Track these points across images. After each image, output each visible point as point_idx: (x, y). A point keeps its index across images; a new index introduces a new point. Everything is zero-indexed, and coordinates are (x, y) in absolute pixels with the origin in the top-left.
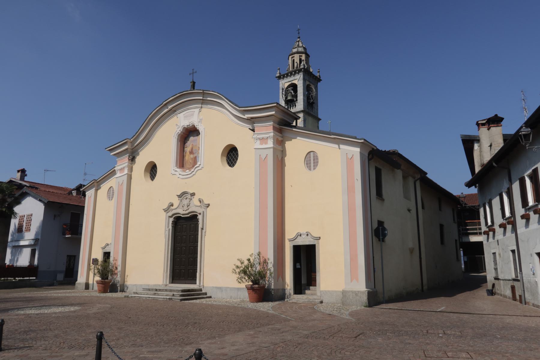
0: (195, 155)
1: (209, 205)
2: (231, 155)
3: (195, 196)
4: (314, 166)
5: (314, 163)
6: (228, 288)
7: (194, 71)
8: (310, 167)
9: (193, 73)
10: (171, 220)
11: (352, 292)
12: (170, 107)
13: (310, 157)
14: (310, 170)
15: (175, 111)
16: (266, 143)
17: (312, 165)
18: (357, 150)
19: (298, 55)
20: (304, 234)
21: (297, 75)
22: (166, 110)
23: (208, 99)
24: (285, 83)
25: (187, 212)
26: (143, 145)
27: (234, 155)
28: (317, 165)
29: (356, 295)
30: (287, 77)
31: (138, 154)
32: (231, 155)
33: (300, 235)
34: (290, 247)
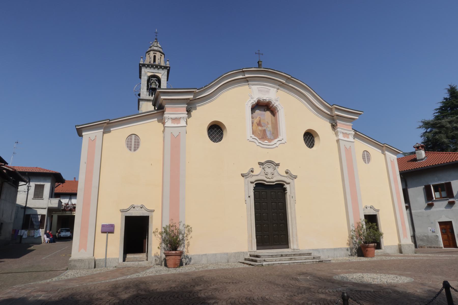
0: (263, 128)
1: (243, 175)
2: (310, 137)
3: (279, 167)
4: (368, 161)
5: (368, 159)
6: (325, 249)
7: (257, 52)
8: (131, 147)
9: (259, 54)
10: (253, 185)
11: (197, 255)
12: (247, 76)
13: (131, 139)
14: (130, 150)
15: (248, 81)
16: (348, 138)
17: (133, 146)
18: (394, 157)
19: (160, 54)
20: (138, 207)
21: (161, 70)
22: (241, 77)
23: (290, 85)
24: (147, 72)
25: (268, 180)
26: (207, 100)
27: (309, 138)
28: (138, 148)
29: (409, 246)
30: (154, 68)
31: (195, 109)
32: (310, 137)
33: (134, 208)
34: (122, 217)
